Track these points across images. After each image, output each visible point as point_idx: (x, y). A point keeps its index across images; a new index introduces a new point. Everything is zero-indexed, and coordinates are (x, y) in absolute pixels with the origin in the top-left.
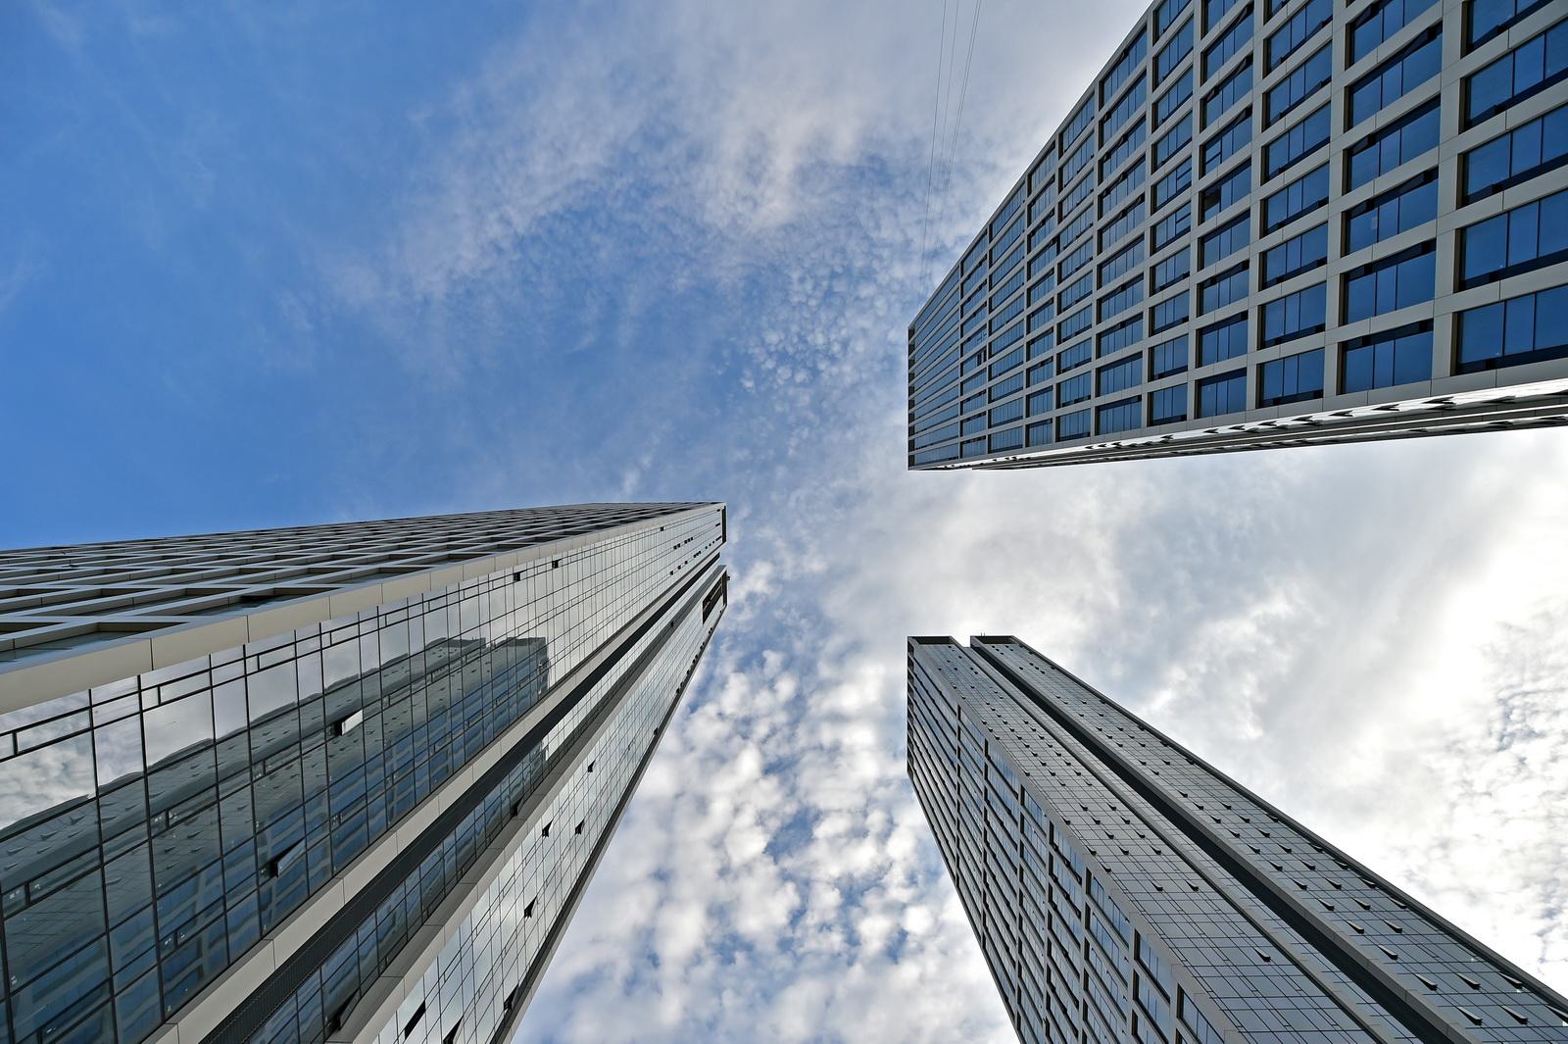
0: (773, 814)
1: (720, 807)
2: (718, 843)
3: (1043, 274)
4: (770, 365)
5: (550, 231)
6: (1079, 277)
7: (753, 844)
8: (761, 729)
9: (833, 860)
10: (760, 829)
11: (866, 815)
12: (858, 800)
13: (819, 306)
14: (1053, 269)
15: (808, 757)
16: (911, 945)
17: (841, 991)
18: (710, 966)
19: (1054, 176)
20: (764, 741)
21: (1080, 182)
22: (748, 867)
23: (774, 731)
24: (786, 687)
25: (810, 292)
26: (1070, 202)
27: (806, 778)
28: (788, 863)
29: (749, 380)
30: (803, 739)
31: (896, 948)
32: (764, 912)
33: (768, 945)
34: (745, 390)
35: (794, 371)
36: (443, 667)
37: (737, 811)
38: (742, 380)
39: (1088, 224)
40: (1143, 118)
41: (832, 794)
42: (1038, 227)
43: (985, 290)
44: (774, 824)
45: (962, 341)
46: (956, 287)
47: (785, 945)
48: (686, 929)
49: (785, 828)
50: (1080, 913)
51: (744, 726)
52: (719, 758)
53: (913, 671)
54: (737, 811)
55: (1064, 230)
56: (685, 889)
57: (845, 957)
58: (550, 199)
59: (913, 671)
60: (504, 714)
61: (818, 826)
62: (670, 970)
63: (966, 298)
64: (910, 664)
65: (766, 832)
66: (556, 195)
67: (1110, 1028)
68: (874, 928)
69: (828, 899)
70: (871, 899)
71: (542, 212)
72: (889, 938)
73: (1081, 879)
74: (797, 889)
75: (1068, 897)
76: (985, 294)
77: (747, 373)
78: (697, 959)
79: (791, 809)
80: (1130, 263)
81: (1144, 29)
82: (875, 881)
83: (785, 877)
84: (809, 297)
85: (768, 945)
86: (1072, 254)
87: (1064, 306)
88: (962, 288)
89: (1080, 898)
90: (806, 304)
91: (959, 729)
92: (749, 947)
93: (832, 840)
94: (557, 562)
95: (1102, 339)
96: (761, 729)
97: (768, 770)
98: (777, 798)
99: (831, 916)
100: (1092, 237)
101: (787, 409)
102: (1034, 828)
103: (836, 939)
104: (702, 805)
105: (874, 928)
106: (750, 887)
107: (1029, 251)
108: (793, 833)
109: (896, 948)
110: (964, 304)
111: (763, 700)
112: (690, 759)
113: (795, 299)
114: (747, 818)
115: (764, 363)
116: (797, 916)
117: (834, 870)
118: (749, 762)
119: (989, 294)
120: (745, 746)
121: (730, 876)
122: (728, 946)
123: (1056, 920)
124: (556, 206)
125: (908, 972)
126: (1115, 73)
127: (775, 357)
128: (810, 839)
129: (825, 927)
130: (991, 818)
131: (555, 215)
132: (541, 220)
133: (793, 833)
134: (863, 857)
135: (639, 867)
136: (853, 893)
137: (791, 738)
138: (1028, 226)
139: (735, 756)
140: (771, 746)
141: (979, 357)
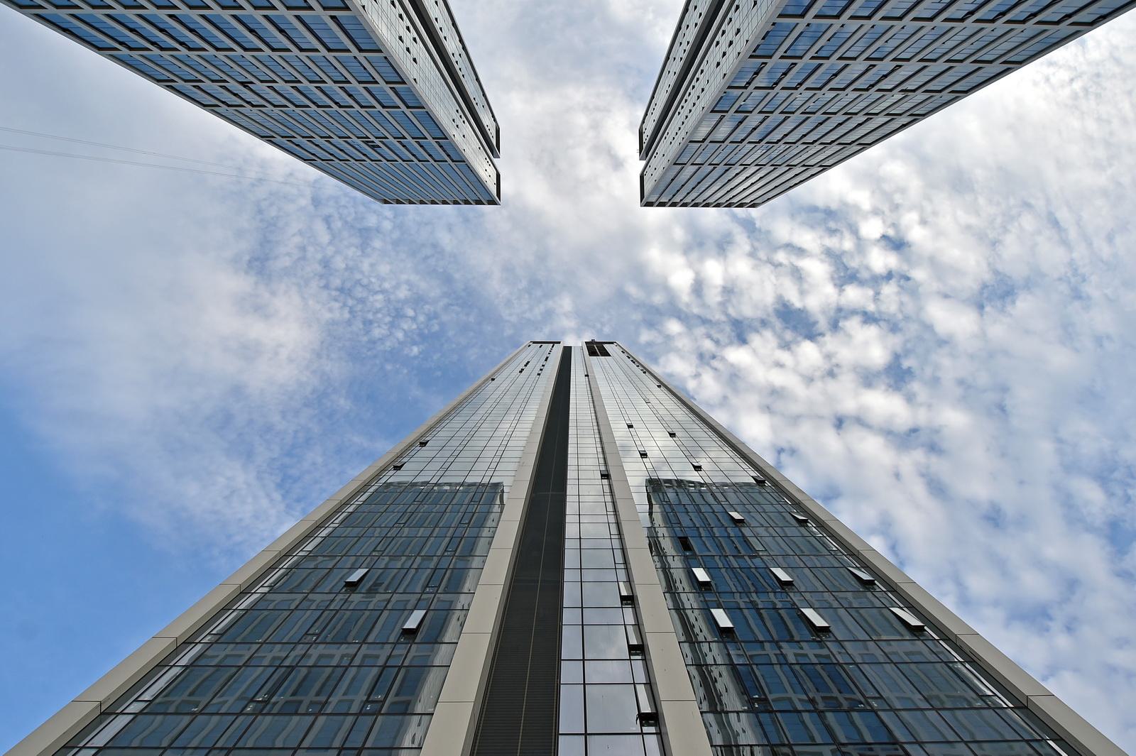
0: (780, 337)
1: (778, 378)
2: (809, 380)
3: (394, 94)
4: (400, 335)
5: (298, 500)
6: (371, 67)
7: (809, 352)
8: (708, 345)
9: (820, 293)
10: (793, 347)
11: (780, 265)
12: (767, 269)
13: (352, 298)
14: (391, 88)
15: (731, 311)
16: (891, 232)
17: (935, 286)
18: (915, 386)
19: (316, 87)
20: (717, 342)
21: (239, 65)
22: (828, 356)
23: (709, 336)
24: (674, 327)
25: (341, 304)
26: (334, 74)
27: (747, 311)
28: (823, 324)
29: (412, 350)
30: (718, 316)
31: (896, 244)
32: (873, 347)
33: (896, 341)
34: (420, 353)
35: (404, 316)
36: (704, 542)
37: (779, 365)
38: (412, 355)
39: (385, 61)
40: (235, 17)
41: (762, 288)
42: (355, 100)
43: (425, 142)
44: (789, 335)
45: (450, 162)
46: (406, 166)
47: (894, 328)
48: (883, 404)
49: (795, 329)
50: (897, 66)
51: (704, 358)
52: (734, 378)
53: (701, 203)
54: (779, 365)
55: (331, 78)
56: (849, 405)
57: (902, 282)
58: (272, 500)
59: (701, 203)
60: (720, 518)
61: (793, 304)
62: (922, 417)
63: (413, 158)
64: (707, 205)
65: (797, 343)
66: (268, 495)
67: (936, 40)
68: (880, 260)
69: (854, 295)
70: (854, 263)
71: (282, 507)
72: (885, 248)
73: (871, 65)
74: (846, 318)
75: (885, 76)
76: (409, 142)
77: (406, 351)
78: (910, 399)
79: (778, 324)
80: (359, 27)
81: (38, 16)
82: (834, 257)
83: (835, 326)
84: (345, 305)
85: (896, 341)
86: (325, 72)
87: (398, 79)
88: (439, 161)
89: (887, 65)
90: (351, 308)
91: (757, 165)
92: (897, 357)
93: (803, 293)
94: (641, 455)
95: (363, 48)
96: (708, 345)
97: (742, 340)
98: (768, 334)
99: (871, 293)
100: (365, 57)
101: (435, 321)
102: (810, 103)
103: (889, 290)
104: (776, 393)
105: (880, 260)
106: (845, 355)
107: (352, 107)
108: (795, 323)
109: (896, 244)
110: (433, 159)
111: (684, 343)
112: (734, 401)
113: (347, 316)
114: (784, 356)
115: (398, 339)
116: (869, 318)
117: (830, 290)
118: (737, 356)
119: (409, 139)
120: (723, 359)
121: (836, 370)
122: (896, 375)
123: (907, 86)
124: (277, 496)
125: (917, 234)
126: (238, 39)
127: (394, 330)
128: (802, 312)
129: (877, 297)
130: (828, 139)
131: (284, 497)
132: (289, 507)
133: (795, 323)
134: (817, 269)
135: (832, 441)
136: (846, 275)
137: (718, 323)
138: (354, 108)
139: (732, 365)
140: (723, 339)
141: (374, 147)
